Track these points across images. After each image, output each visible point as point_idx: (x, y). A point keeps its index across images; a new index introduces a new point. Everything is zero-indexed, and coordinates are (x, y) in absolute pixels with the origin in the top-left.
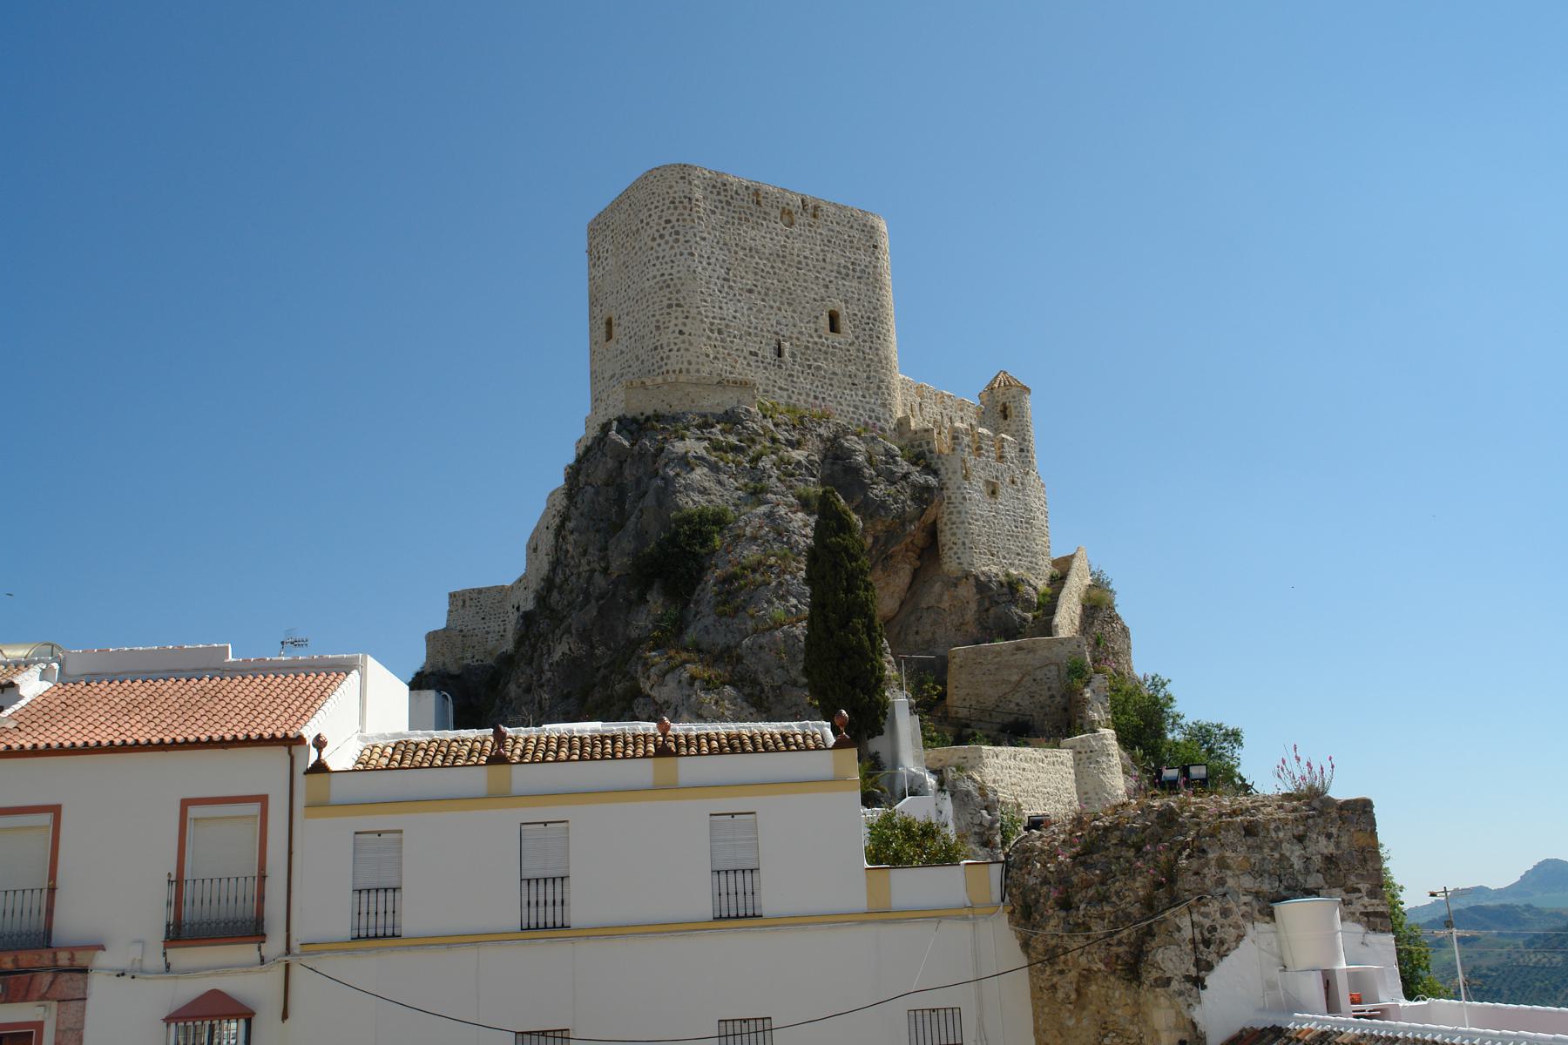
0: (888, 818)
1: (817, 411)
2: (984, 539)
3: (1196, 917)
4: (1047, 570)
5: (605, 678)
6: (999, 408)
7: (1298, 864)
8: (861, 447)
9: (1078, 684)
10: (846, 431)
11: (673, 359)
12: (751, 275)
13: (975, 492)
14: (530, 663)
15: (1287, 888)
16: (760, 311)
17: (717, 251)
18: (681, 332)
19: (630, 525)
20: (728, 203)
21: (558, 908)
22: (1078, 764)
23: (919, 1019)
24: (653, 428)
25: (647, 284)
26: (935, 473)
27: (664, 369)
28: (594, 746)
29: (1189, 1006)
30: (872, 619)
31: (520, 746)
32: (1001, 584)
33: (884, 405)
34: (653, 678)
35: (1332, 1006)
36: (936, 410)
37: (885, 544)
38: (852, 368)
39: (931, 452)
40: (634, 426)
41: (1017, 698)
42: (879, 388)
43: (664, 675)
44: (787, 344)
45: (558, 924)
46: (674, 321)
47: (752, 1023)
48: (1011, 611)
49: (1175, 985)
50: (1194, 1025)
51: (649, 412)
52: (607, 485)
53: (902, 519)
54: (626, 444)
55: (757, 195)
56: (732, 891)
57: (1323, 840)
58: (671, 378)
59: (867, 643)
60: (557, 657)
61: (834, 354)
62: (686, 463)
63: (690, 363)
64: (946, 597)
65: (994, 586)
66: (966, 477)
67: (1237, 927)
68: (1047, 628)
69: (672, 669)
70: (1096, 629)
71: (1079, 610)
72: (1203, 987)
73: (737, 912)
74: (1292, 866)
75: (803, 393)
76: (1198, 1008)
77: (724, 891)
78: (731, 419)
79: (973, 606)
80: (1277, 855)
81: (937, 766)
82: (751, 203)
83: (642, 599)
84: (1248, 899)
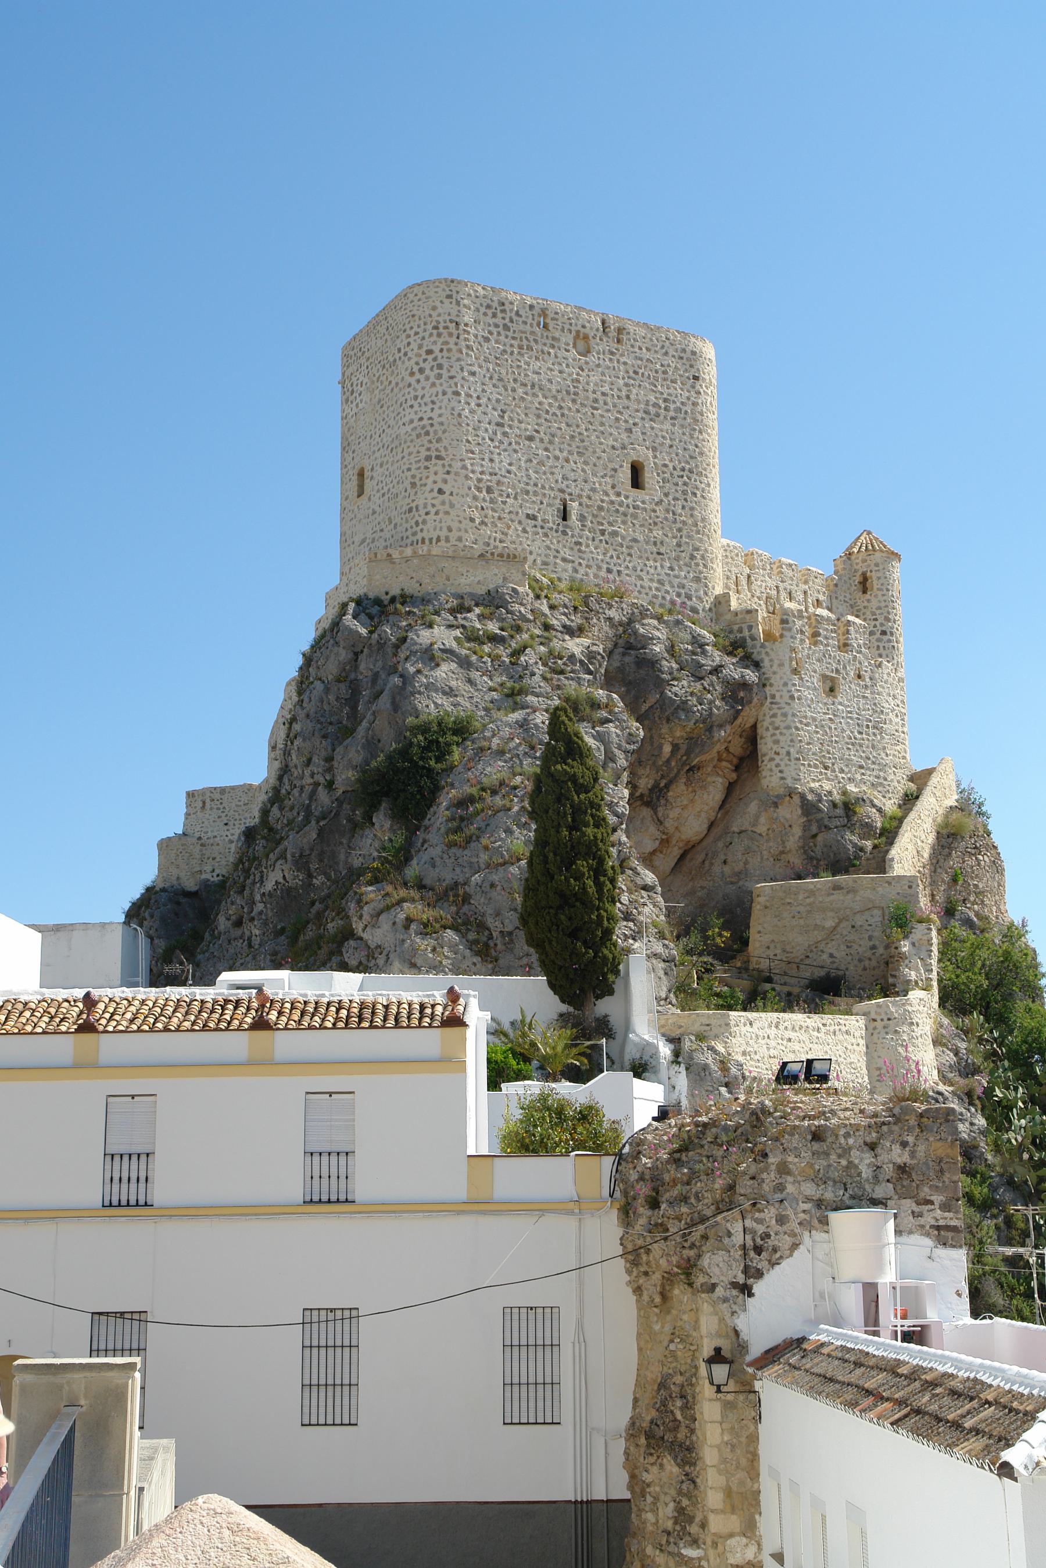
0: (543, 1098)
1: (609, 588)
2: (816, 748)
3: (748, 1223)
4: (899, 784)
5: (319, 915)
6: (858, 579)
7: (866, 1172)
8: (661, 634)
9: (896, 932)
10: (644, 614)
11: (430, 525)
12: (532, 418)
13: (807, 688)
14: (241, 892)
15: (852, 1197)
16: (541, 463)
17: (489, 388)
18: (441, 491)
19: (361, 730)
20: (506, 328)
21: (142, 1185)
22: (870, 1032)
23: (516, 1317)
24: (396, 612)
25: (403, 430)
26: (757, 665)
27: (419, 536)
28: (213, 1011)
29: (733, 1313)
30: (601, 861)
31: (133, 1009)
32: (835, 805)
33: (697, 579)
34: (366, 917)
35: (872, 1321)
36: (770, 583)
37: (688, 753)
38: (658, 533)
39: (753, 638)
40: (374, 608)
41: (831, 948)
42: (692, 557)
43: (379, 914)
44: (575, 504)
45: (142, 1202)
46: (432, 478)
47: (315, 1313)
48: (840, 840)
49: (719, 1291)
50: (737, 1333)
51: (395, 591)
52: (339, 681)
53: (709, 724)
54: (363, 631)
55: (544, 316)
56: (325, 1174)
57: (897, 1149)
58: (422, 550)
59: (592, 890)
60: (269, 886)
61: (635, 516)
62: (430, 657)
63: (450, 530)
64: (762, 820)
65: (824, 807)
66: (795, 671)
67: (793, 1235)
68: (881, 864)
69: (388, 908)
70: (954, 862)
71: (931, 839)
72: (751, 1295)
73: (328, 1198)
74: (859, 1174)
75: (592, 565)
76: (742, 1315)
77: (316, 1175)
78: (493, 602)
79: (797, 831)
80: (844, 1163)
81: (676, 1033)
82: (531, 326)
83: (369, 819)
84: (807, 1206)
